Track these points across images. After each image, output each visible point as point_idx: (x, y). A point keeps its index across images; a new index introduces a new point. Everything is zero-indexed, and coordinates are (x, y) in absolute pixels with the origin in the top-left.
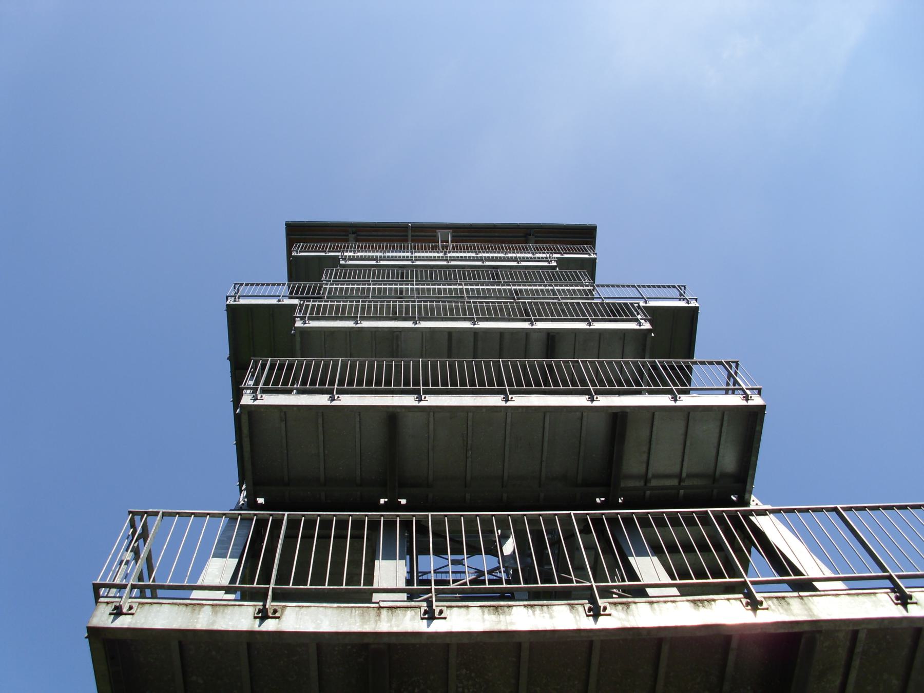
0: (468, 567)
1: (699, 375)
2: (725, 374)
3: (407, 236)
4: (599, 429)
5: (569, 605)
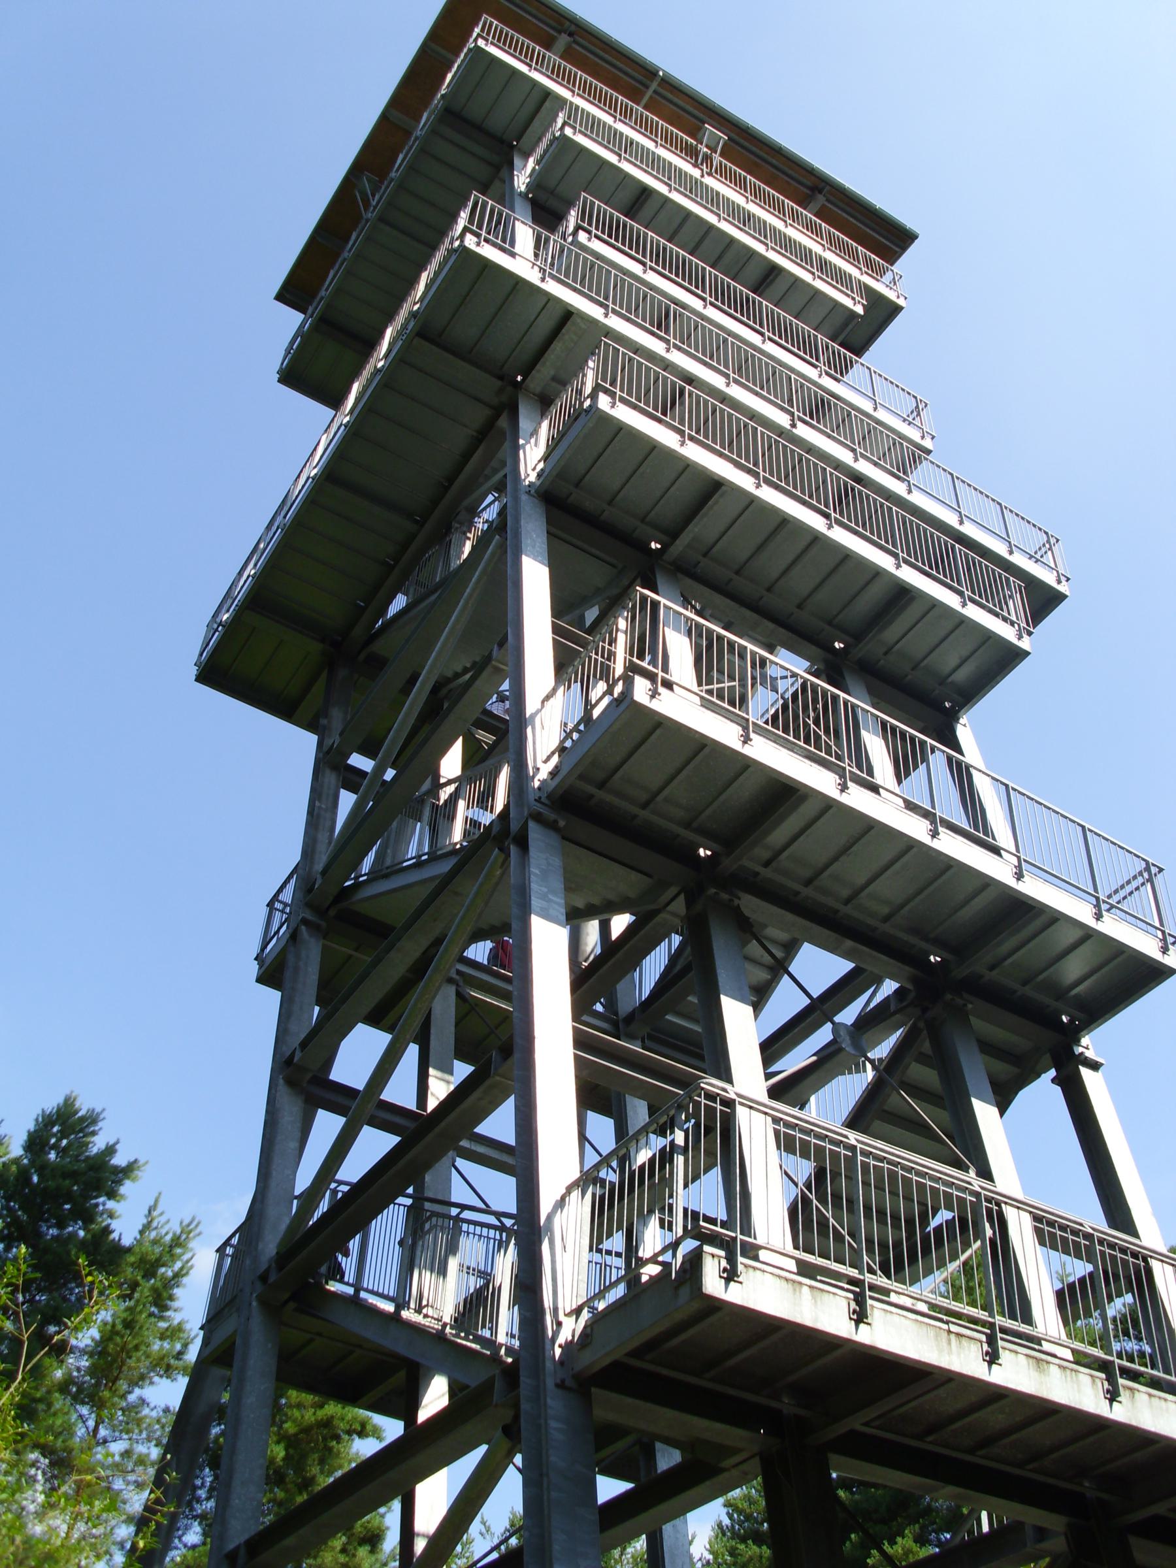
0: (350, 956)
1: (856, 373)
2: (914, 405)
3: (647, 87)
4: (875, 594)
5: (1092, 1376)
